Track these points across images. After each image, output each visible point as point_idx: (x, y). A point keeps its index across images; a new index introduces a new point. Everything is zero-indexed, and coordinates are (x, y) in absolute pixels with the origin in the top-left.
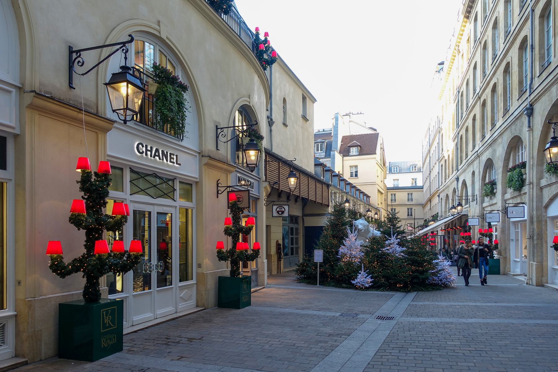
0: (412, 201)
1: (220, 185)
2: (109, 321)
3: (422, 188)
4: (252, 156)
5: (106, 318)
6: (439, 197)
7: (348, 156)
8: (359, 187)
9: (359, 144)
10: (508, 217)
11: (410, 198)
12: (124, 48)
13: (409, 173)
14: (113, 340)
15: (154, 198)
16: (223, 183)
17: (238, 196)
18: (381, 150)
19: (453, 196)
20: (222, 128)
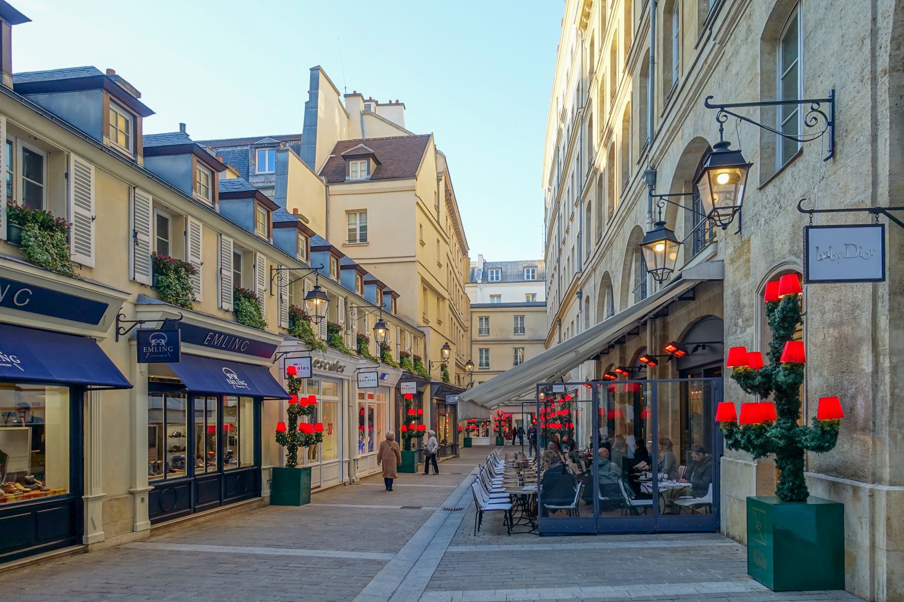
0: (524, 332)
3: (544, 305)
6: (580, 297)
7: (343, 182)
8: (375, 272)
9: (372, 151)
10: (880, 276)
11: (519, 326)
13: (521, 282)
18: (438, 185)
19: (628, 267)
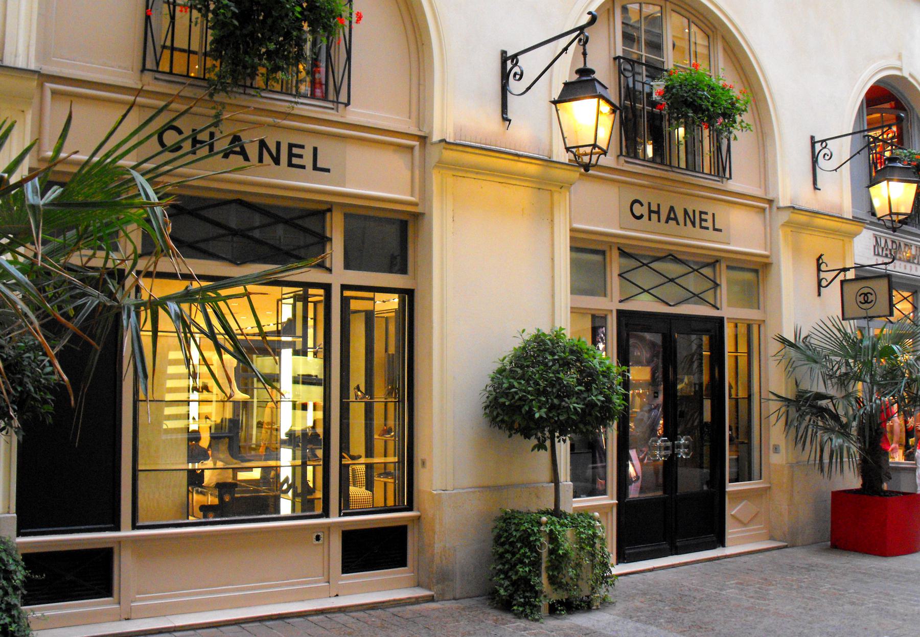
1: (823, 267)
12: (582, 37)
15: (670, 305)
16: (832, 263)
17: (866, 291)
20: (822, 141)
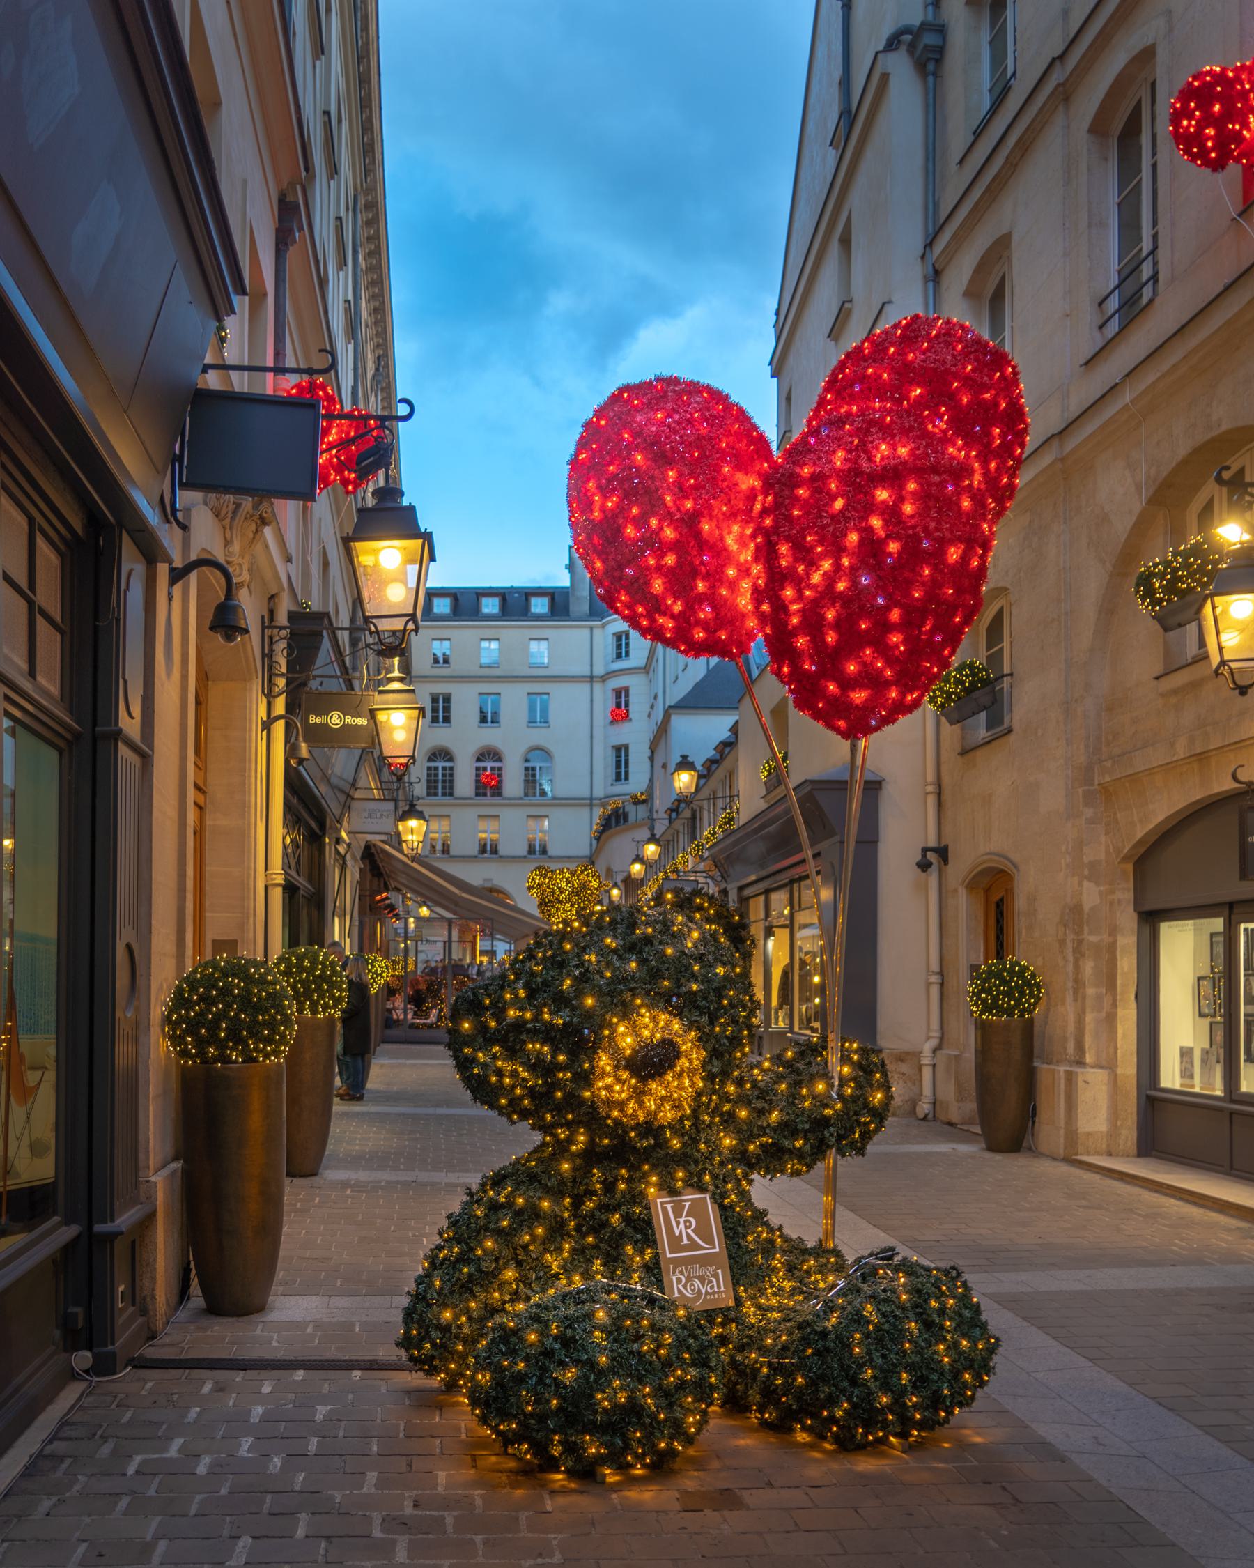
2: (689, 1231)
4: (397, 728)
5: (678, 1223)
14: (711, 1282)
